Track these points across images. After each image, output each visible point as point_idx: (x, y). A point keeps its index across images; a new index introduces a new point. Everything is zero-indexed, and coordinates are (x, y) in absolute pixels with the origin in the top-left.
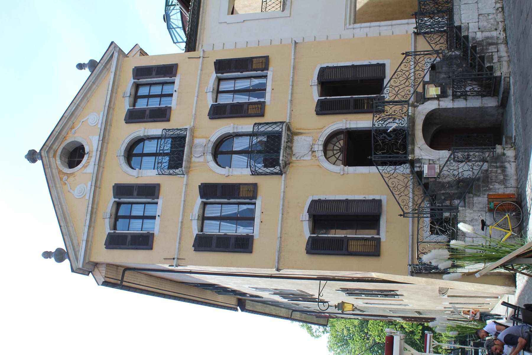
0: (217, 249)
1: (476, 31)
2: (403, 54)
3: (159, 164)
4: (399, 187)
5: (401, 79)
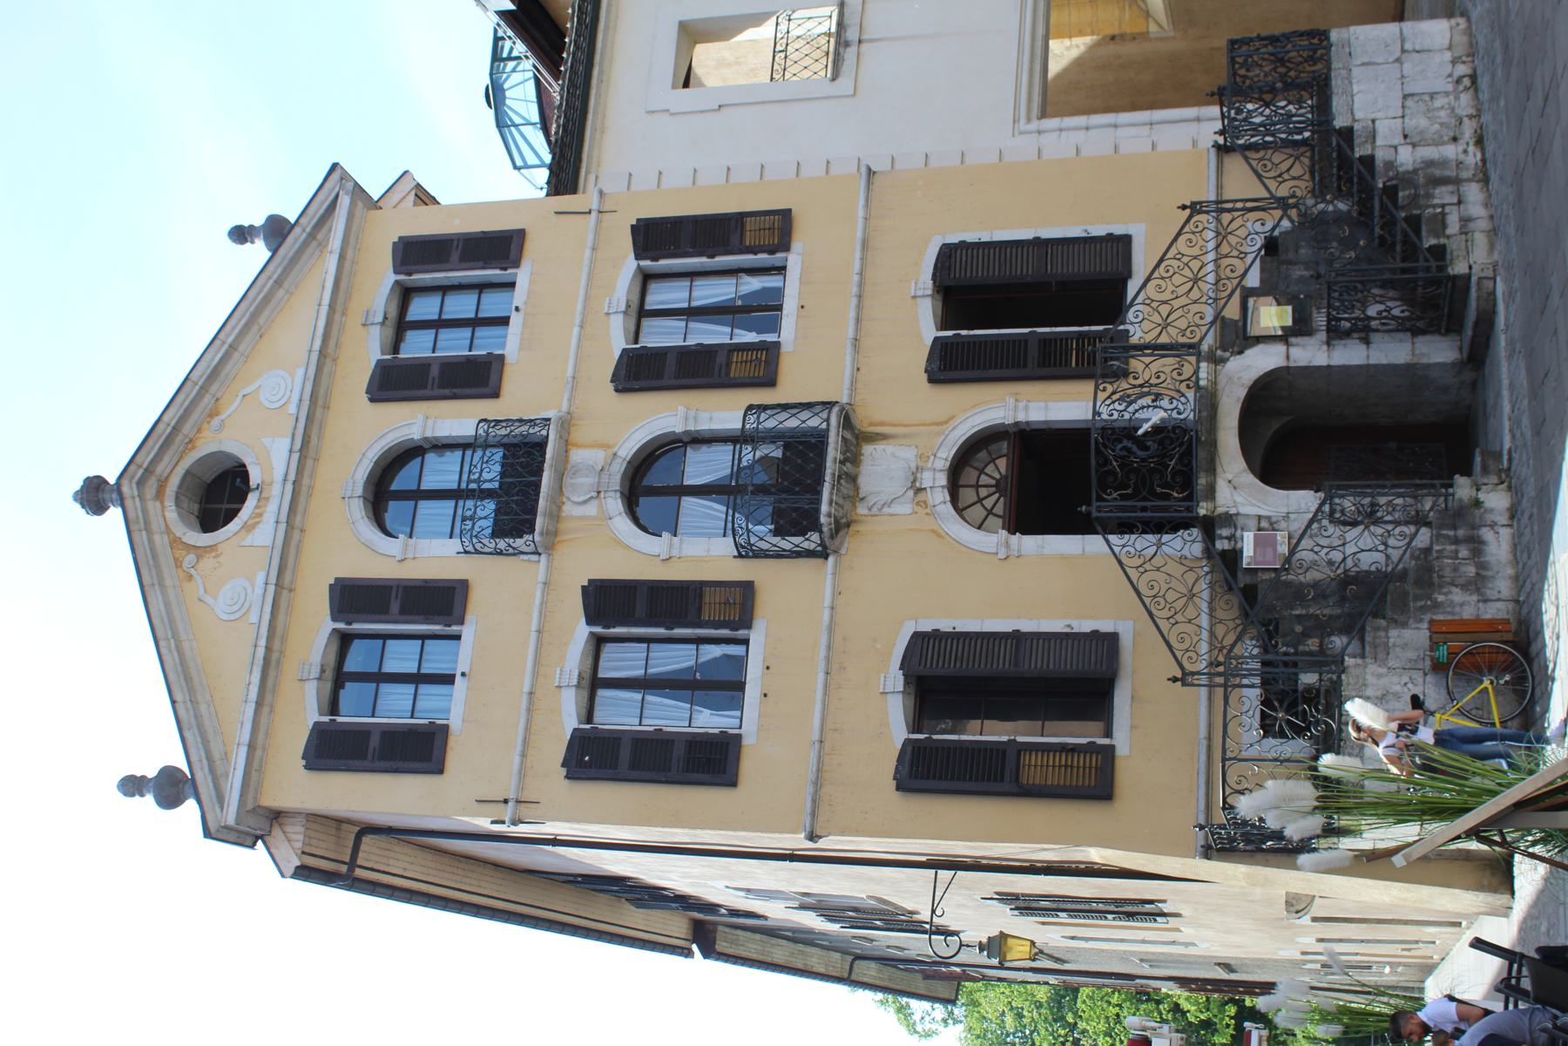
0: (635, 774)
1: (1395, 142)
2: (1184, 207)
3: (468, 522)
4: (1171, 596)
5: (1177, 279)
